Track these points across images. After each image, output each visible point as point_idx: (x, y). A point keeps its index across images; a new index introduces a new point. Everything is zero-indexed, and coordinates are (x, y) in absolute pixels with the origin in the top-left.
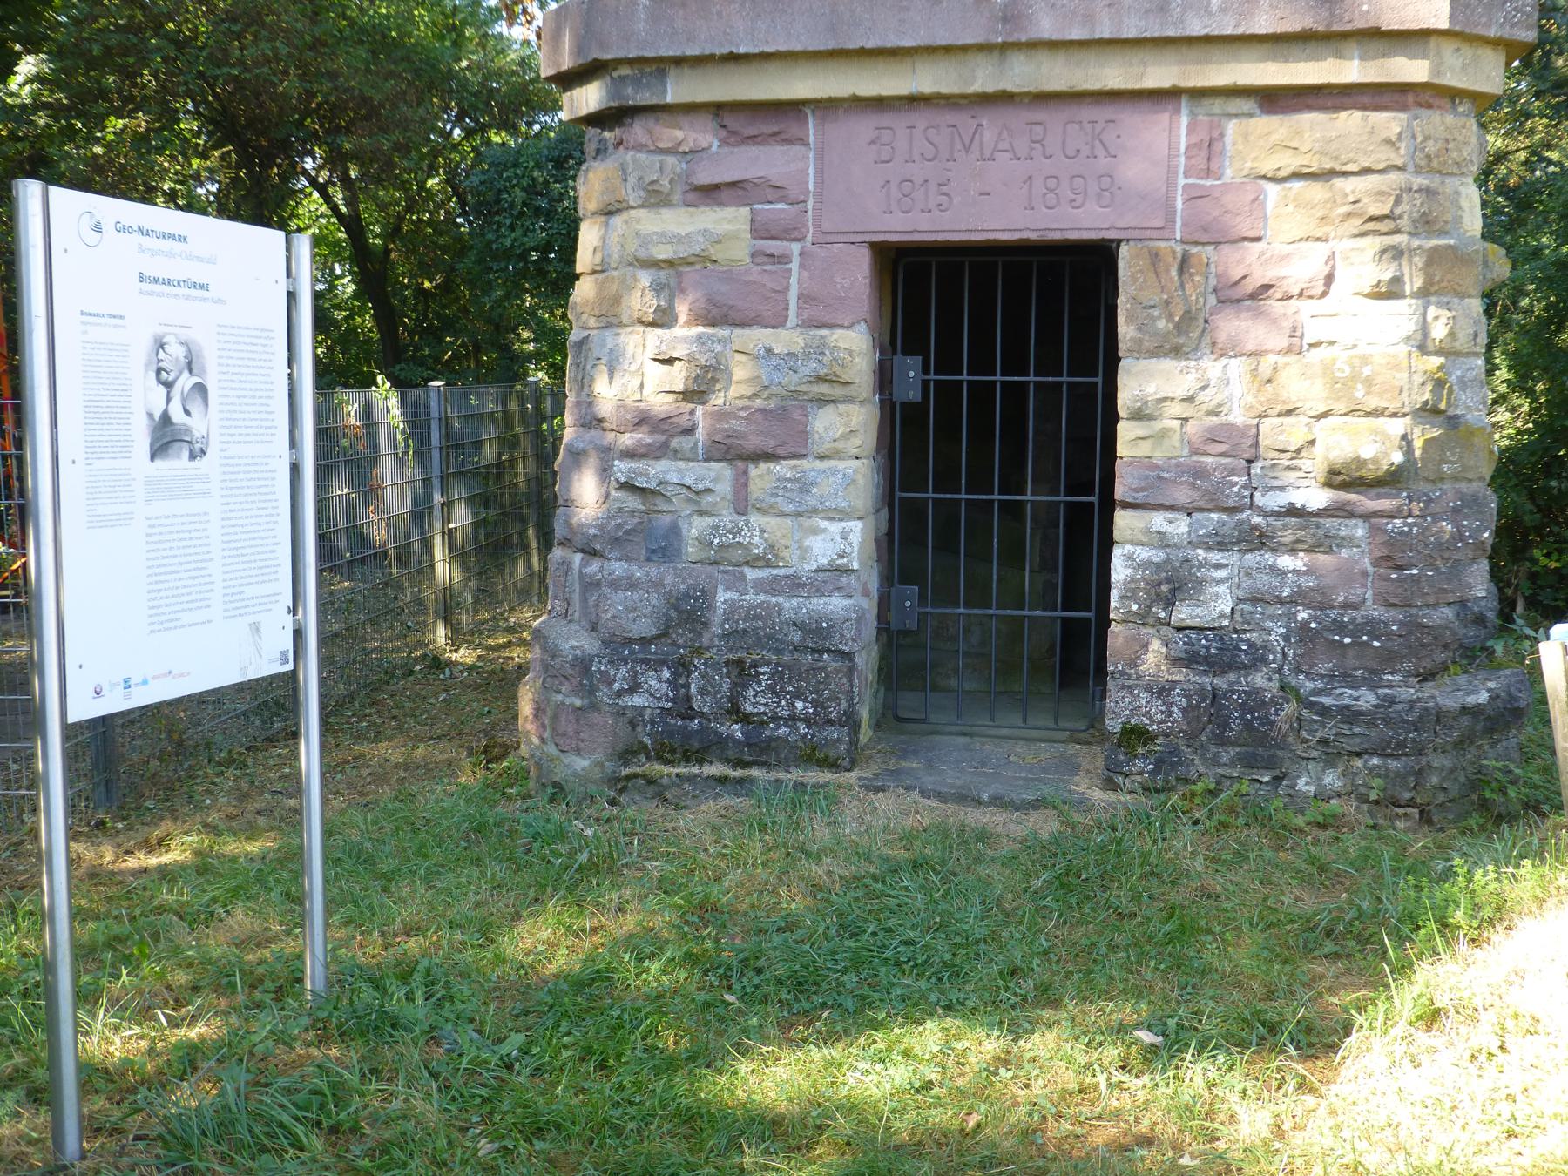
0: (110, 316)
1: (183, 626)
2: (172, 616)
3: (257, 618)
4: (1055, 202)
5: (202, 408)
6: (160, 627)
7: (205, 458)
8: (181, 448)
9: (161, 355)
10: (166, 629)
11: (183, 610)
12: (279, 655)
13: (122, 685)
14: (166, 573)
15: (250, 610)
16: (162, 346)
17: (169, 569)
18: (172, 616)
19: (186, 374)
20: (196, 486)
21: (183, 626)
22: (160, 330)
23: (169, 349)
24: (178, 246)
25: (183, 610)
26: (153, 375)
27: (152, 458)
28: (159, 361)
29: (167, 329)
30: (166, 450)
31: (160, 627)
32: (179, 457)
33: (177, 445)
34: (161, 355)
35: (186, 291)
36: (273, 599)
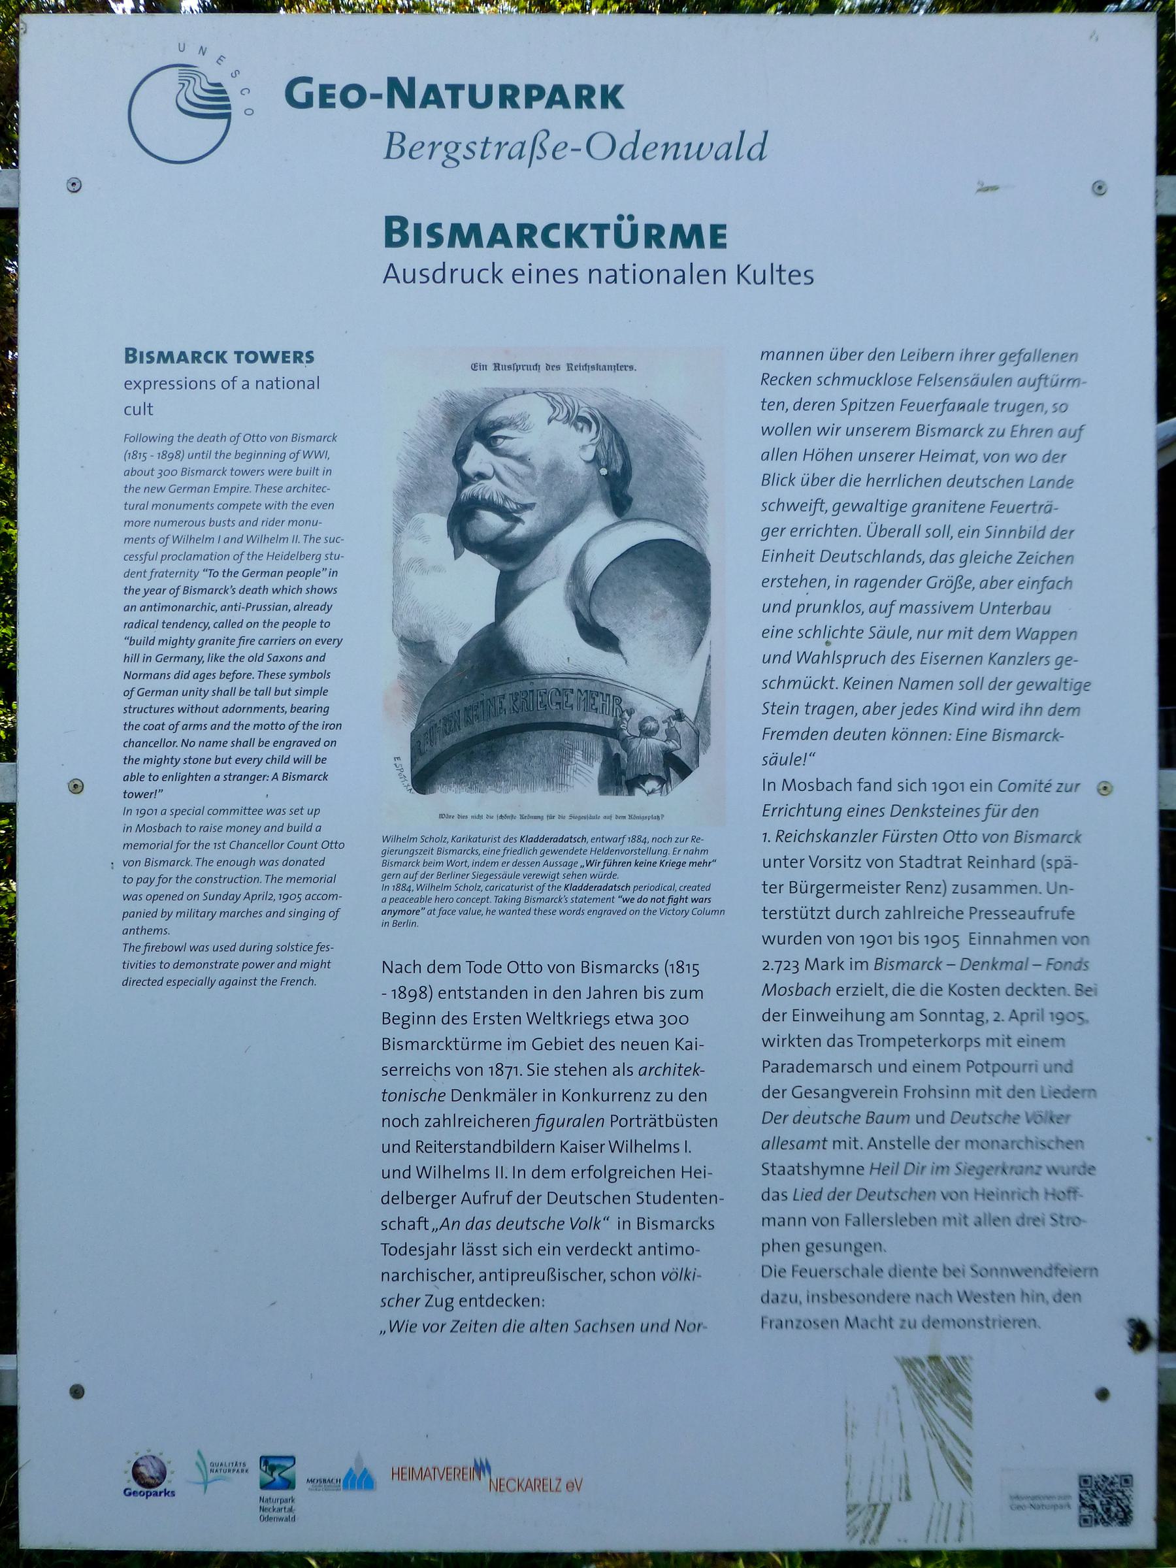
0: (251, 357)
1: (543, 1326)
2: (1031, 596)
3: (950, 1344)
4: (1063, 586)
5: (675, 621)
6: (438, 1315)
7: (682, 790)
8: (564, 754)
9: (479, 458)
10: (459, 1327)
11: (551, 1275)
12: (1073, 1490)
13: (256, 1474)
14: (466, 1147)
15: (916, 1311)
16: (486, 434)
17: (491, 1135)
18: (1031, 596)
19: (598, 515)
20: (626, 876)
21: (543, 1326)
22: (474, 385)
23: (516, 441)
24: (703, 257)
25: (551, 1275)
26: (436, 525)
27: (422, 781)
28: (466, 480)
29: (492, 380)
30: (492, 755)
31: (438, 1315)
32: (553, 777)
33: (540, 742)
34: (479, 458)
35: (611, 256)
36: (1049, 1286)
